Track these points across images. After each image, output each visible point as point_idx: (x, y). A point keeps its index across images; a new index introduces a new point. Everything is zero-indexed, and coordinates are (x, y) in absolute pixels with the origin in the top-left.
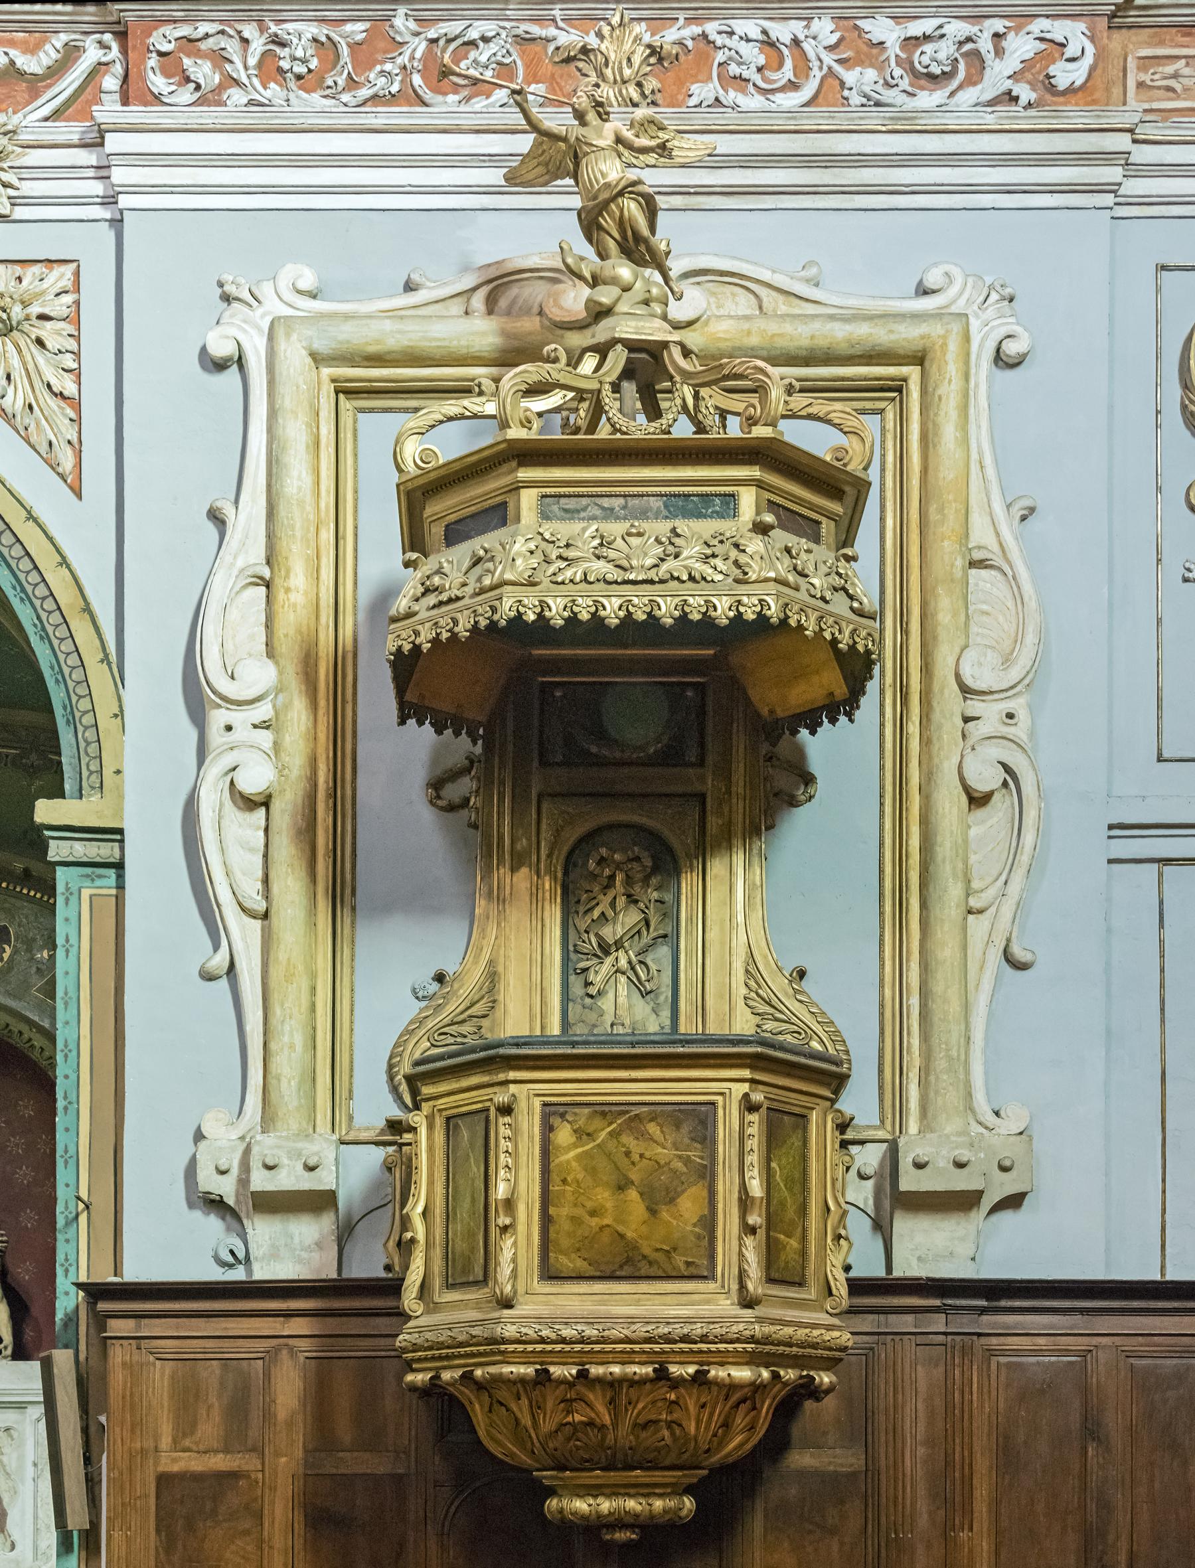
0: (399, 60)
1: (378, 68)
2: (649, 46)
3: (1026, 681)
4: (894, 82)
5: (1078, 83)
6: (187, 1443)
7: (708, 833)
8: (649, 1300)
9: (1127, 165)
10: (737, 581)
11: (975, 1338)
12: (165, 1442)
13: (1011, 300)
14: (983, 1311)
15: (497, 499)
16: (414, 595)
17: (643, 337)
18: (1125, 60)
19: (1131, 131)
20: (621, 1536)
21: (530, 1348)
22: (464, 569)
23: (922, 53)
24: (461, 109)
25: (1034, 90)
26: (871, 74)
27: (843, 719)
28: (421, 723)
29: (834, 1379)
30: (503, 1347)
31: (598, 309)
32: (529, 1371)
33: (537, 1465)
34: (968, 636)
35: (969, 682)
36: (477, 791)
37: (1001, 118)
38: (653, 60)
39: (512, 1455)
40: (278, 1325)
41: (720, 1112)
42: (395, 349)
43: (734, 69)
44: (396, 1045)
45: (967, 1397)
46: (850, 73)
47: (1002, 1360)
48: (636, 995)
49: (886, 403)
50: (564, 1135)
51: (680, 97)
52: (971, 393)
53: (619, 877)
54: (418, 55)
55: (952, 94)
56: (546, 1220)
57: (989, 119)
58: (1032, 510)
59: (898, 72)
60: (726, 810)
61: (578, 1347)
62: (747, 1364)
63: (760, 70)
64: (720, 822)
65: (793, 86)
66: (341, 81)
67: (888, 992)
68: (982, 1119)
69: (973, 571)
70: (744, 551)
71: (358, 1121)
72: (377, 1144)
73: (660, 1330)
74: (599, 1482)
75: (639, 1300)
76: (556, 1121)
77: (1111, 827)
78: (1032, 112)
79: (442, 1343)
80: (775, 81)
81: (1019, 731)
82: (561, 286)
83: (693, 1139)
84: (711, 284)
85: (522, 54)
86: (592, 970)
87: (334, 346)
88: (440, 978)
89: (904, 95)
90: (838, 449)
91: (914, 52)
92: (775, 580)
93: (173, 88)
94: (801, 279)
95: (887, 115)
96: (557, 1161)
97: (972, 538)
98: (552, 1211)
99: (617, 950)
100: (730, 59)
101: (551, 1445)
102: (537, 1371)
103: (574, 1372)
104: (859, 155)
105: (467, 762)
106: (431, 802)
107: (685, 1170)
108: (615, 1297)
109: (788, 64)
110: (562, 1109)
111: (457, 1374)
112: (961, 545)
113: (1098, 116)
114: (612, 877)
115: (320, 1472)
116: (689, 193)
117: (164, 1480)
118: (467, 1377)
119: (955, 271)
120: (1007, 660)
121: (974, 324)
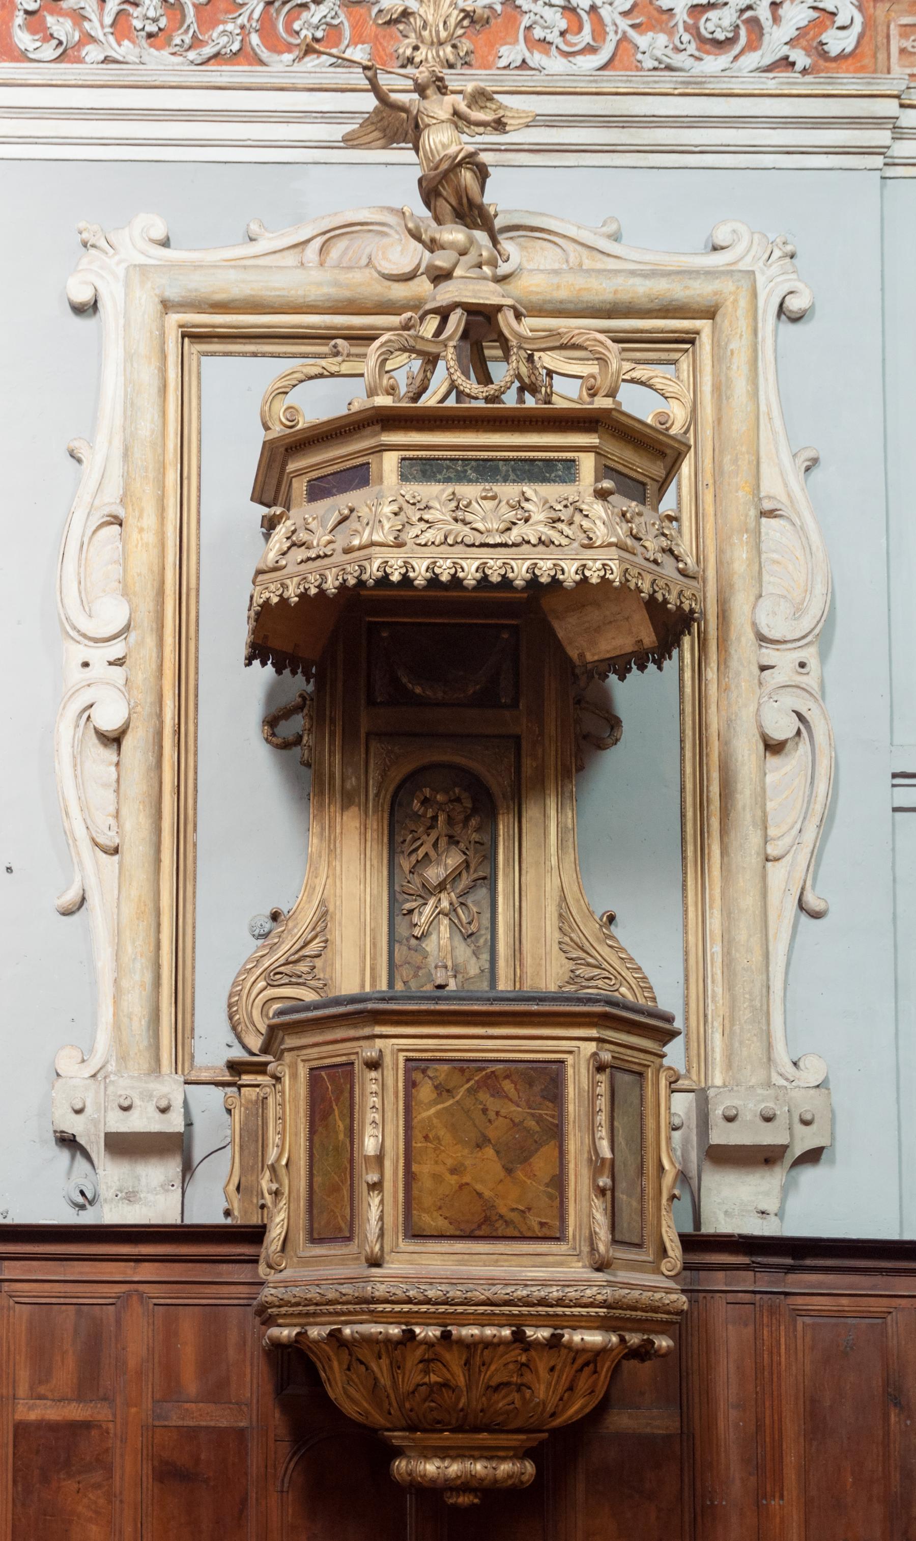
0: (239, 21)
1: (221, 28)
2: (463, 10)
3: (817, 631)
4: (682, 47)
5: (848, 50)
6: (42, 1390)
7: (523, 775)
8: (506, 1261)
9: (894, 128)
10: (584, 546)
11: (782, 1297)
12: (23, 1389)
13: (792, 257)
14: (790, 1269)
15: (360, 459)
16: (279, 549)
17: (481, 301)
18: (888, 27)
19: (898, 97)
20: (464, 1500)
21: (397, 1308)
22: (330, 524)
23: (707, 20)
24: (295, 68)
25: (809, 56)
26: (662, 39)
27: (651, 667)
28: (264, 664)
29: (671, 1343)
30: (372, 1306)
31: (438, 273)
32: (395, 1331)
33: (388, 1425)
34: (761, 586)
35: (765, 631)
36: (309, 730)
37: (782, 83)
38: (466, 23)
39: (367, 1414)
40: (129, 1271)
41: (570, 1071)
42: (238, 297)
43: (538, 33)
44: (235, 984)
45: (775, 1358)
46: (644, 38)
47: (808, 1320)
48: (458, 939)
49: (680, 354)
50: (425, 1092)
51: (491, 58)
52: (759, 347)
53: (441, 818)
54: (256, 15)
55: (736, 58)
56: (410, 1177)
57: (771, 83)
58: (815, 461)
59: (686, 37)
60: (540, 751)
61: (442, 1309)
62: (597, 1328)
63: (562, 34)
64: (534, 765)
65: (590, 49)
66: (188, 39)
67: (691, 939)
68: (783, 1071)
69: (764, 520)
70: (587, 516)
71: (198, 1061)
72: (217, 1084)
73: (519, 1293)
74: (447, 1444)
75: (497, 1261)
76: (417, 1076)
77: (895, 776)
78: (809, 78)
79: (310, 1300)
80: (575, 45)
81: (810, 681)
82: (386, 240)
83: (544, 1097)
84: (522, 239)
85: (349, 16)
86: (416, 911)
87: (183, 294)
88: (275, 916)
89: (692, 59)
90: (660, 414)
91: (699, 19)
92: (616, 545)
93: (38, 44)
94: (602, 235)
95: (680, 79)
96: (419, 1117)
97: (762, 488)
98: (415, 1168)
99: (440, 892)
100: (535, 23)
101: (408, 1405)
102: (403, 1331)
103: (438, 1333)
104: (654, 116)
105: (299, 700)
106: (267, 740)
107: (537, 1129)
108: (474, 1257)
109: (587, 28)
110: (423, 1065)
111: (324, 1331)
112: (754, 495)
113: (869, 83)
114: (435, 818)
115: (166, 1423)
116: (500, 150)
117: (21, 1430)
118: (335, 1335)
119: (742, 229)
120: (798, 611)
121: (761, 280)
